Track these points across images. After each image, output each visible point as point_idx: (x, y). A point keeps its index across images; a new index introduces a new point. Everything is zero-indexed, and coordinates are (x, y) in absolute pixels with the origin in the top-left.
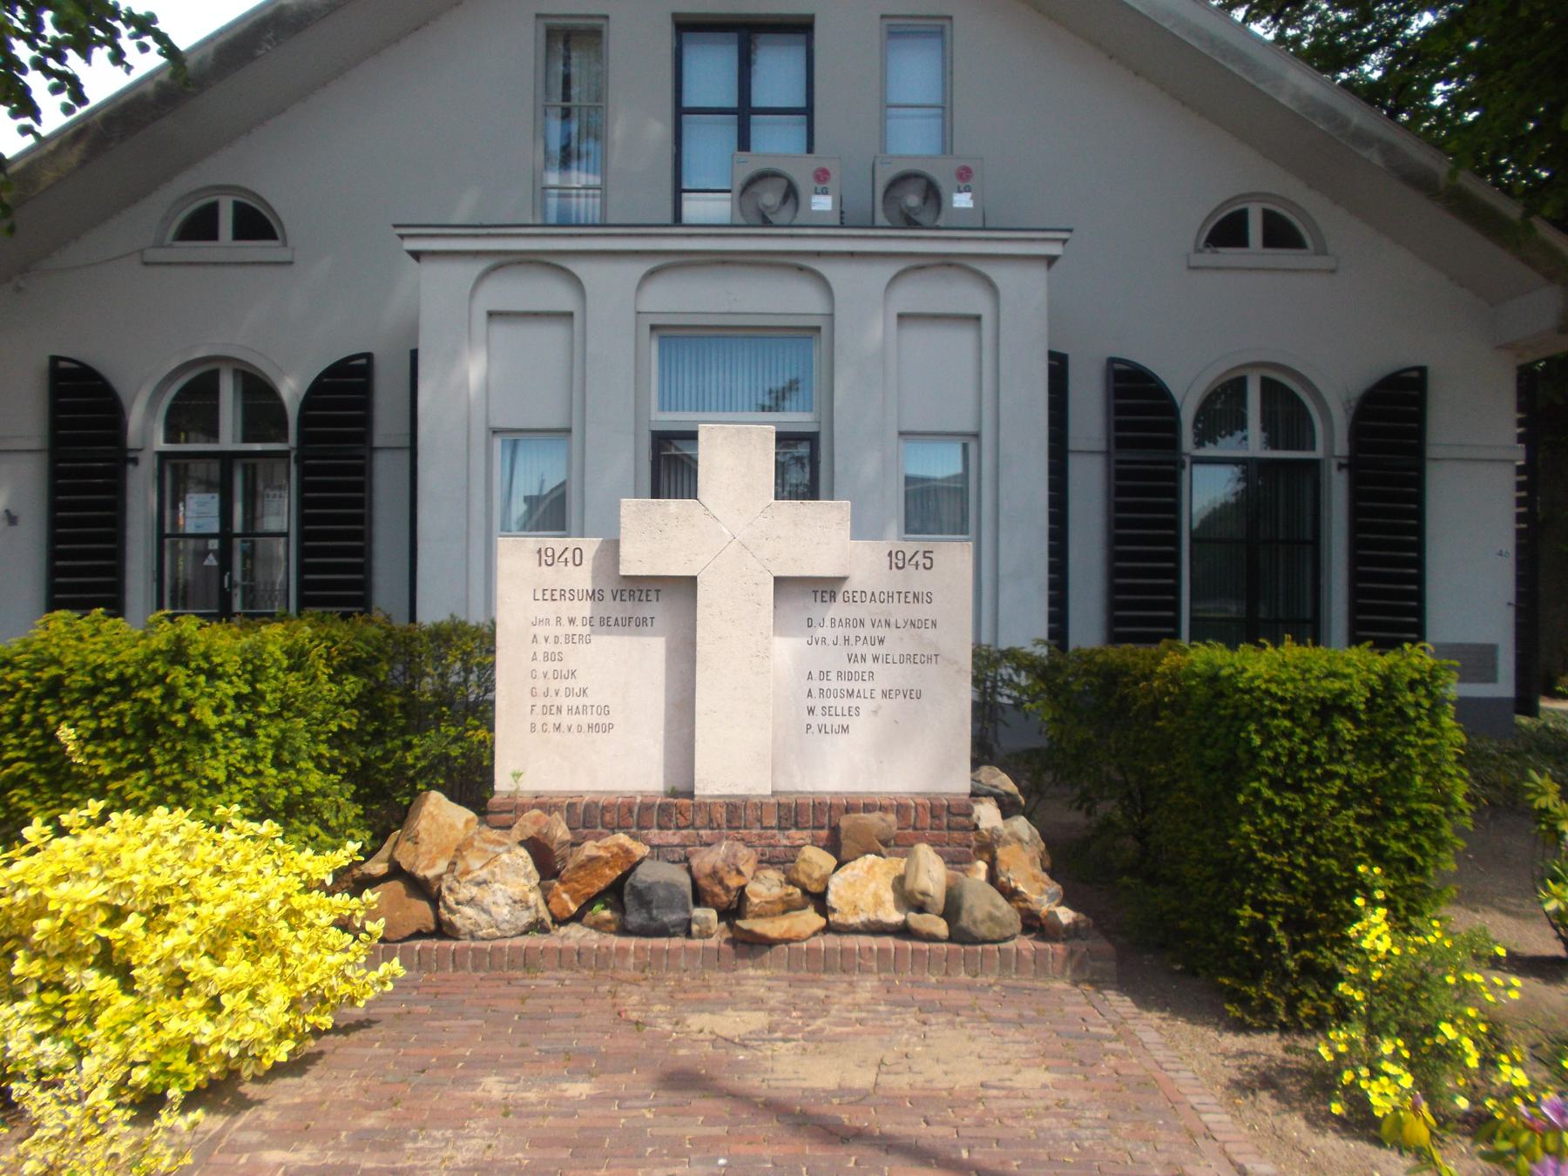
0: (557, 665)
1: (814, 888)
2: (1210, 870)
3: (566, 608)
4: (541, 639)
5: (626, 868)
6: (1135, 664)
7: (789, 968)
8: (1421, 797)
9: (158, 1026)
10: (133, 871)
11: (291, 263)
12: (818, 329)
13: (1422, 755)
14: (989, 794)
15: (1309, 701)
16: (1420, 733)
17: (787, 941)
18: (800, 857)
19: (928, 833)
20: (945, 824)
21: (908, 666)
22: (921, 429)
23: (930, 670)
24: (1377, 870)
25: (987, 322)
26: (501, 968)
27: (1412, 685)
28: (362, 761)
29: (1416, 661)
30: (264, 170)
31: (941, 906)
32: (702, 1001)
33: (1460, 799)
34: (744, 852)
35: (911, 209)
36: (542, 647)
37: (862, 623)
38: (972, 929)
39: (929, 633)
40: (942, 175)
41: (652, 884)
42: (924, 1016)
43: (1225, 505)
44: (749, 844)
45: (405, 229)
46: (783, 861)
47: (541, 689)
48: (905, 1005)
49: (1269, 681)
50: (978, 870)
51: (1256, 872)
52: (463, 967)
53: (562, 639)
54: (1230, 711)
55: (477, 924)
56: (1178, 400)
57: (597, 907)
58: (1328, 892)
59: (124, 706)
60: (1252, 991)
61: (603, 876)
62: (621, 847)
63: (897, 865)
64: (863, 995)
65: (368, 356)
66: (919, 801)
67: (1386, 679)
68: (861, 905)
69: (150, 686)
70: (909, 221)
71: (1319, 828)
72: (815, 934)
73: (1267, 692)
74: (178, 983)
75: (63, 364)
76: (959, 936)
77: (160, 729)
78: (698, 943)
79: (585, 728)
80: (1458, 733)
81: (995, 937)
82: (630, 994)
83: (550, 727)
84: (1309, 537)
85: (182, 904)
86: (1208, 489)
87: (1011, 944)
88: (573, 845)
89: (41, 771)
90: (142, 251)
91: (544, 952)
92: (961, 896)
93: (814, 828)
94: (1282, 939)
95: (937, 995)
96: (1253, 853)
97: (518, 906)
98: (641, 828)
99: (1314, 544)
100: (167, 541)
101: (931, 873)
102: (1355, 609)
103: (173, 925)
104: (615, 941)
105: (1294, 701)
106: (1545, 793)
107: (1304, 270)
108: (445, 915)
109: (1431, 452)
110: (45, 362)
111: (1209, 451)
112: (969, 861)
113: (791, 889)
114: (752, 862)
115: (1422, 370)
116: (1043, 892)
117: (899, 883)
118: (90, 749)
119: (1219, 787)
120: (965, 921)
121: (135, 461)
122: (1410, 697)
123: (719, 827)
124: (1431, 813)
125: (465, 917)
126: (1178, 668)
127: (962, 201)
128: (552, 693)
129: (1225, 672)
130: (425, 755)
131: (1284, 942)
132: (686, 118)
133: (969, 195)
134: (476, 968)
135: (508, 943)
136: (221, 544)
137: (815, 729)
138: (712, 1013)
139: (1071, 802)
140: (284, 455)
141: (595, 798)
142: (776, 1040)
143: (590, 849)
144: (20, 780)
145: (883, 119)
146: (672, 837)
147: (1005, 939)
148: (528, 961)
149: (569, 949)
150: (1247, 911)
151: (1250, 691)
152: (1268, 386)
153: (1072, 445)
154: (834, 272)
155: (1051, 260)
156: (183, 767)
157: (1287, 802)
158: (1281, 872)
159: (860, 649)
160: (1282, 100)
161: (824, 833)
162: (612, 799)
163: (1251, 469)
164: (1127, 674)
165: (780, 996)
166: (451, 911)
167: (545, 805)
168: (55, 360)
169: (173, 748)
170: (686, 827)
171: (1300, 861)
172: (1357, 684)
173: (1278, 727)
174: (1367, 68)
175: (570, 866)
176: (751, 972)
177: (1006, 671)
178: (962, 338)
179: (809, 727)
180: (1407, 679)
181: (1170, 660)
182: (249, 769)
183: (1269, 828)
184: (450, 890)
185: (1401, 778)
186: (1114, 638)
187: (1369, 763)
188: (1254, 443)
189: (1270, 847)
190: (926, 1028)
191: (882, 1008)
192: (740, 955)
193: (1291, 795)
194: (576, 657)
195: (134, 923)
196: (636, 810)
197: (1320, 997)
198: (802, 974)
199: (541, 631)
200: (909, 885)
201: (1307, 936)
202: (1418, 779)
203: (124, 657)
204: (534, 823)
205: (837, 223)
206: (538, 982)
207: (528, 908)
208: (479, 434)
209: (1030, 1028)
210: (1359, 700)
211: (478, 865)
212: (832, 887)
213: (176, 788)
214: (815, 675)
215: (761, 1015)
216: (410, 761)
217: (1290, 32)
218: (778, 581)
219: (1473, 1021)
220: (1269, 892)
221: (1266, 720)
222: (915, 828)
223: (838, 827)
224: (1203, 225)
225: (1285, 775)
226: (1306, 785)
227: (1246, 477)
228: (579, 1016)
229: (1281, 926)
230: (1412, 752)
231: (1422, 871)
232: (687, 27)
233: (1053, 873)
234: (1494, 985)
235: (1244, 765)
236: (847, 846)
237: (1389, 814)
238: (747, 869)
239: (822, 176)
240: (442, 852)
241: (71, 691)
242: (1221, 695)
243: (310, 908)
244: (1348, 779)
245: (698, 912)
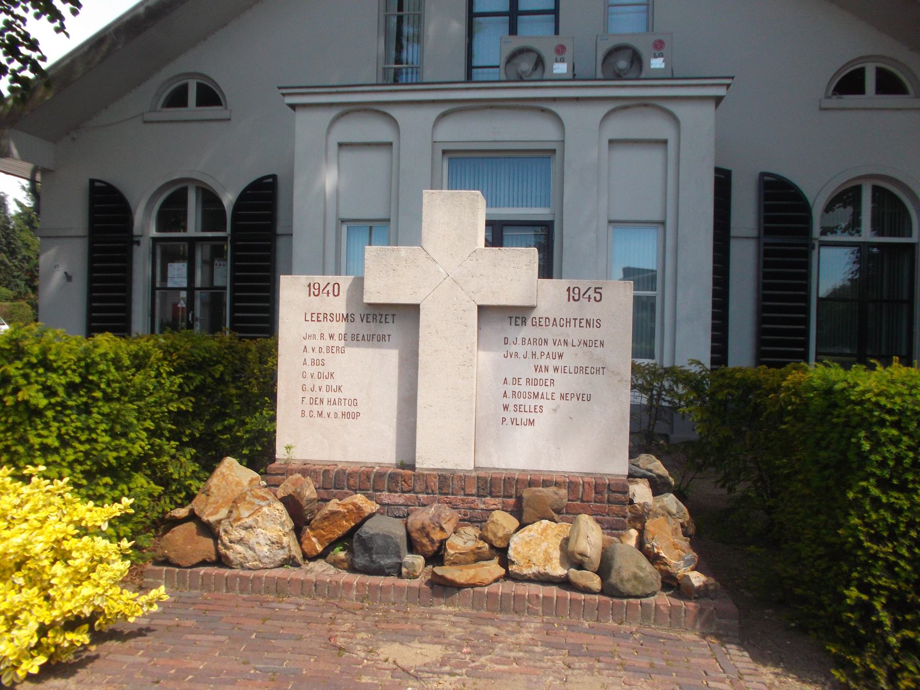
0: (321, 369)
1: (499, 544)
2: (821, 550)
3: (328, 327)
4: (309, 349)
5: (358, 521)
6: (767, 380)
11: (229, 119)
12: (554, 151)
14: (643, 476)
17: (473, 586)
18: (490, 519)
20: (603, 499)
21: (581, 376)
23: (598, 378)
25: (671, 145)
30: (214, 62)
31: (596, 565)
32: (396, 632)
34: (447, 512)
35: (621, 70)
36: (310, 356)
37: (546, 342)
38: (620, 586)
40: (643, 47)
42: (570, 659)
43: (843, 288)
44: (455, 507)
45: (286, 90)
48: (558, 647)
50: (631, 536)
51: (862, 558)
52: (233, 590)
53: (324, 350)
54: (842, 420)
55: (245, 558)
56: (811, 201)
60: (857, 660)
62: (354, 504)
63: (563, 528)
64: (525, 636)
65: (274, 177)
66: (586, 479)
68: (534, 560)
73: (877, 404)
75: (97, 184)
76: (608, 590)
78: (405, 582)
79: (340, 415)
81: (638, 593)
82: (345, 621)
83: (315, 414)
84: (905, 297)
86: (833, 270)
87: (651, 600)
90: (143, 114)
91: (290, 582)
92: (612, 558)
93: (504, 497)
94: (885, 618)
95: (585, 640)
96: (861, 542)
97: (275, 546)
98: (376, 490)
100: (157, 292)
101: (590, 537)
104: (345, 576)
105: (902, 412)
107: (905, 109)
112: (624, 528)
113: (481, 544)
116: (680, 558)
120: (614, 579)
121: (138, 243)
123: (433, 493)
125: (236, 552)
126: (800, 383)
127: (657, 63)
128: (317, 389)
129: (838, 387)
131: (888, 622)
132: (477, 19)
133: (662, 59)
135: (266, 573)
136: (188, 295)
137: (508, 421)
138: (402, 643)
139: (717, 482)
140: (225, 239)
142: (443, 673)
143: (333, 505)
145: (606, 15)
146: (399, 498)
148: (279, 588)
149: (309, 581)
150: (853, 593)
151: (861, 403)
152: (877, 191)
153: (733, 232)
154: (565, 112)
155: (718, 100)
157: (892, 500)
158: (886, 560)
159: (543, 362)
161: (512, 501)
164: (759, 388)
165: (459, 631)
166: (227, 548)
167: (306, 470)
168: (92, 181)
170: (409, 492)
171: (904, 552)
173: (886, 435)
175: (318, 517)
176: (444, 608)
178: (654, 156)
179: (504, 420)
182: (83, 438)
183: (876, 522)
184: (226, 531)
186: (759, 363)
189: (877, 538)
190: (570, 671)
191: (537, 649)
192: (436, 594)
193: (896, 494)
194: (334, 362)
196: (372, 476)
199: (310, 343)
200: (571, 547)
201: (908, 617)
204: (293, 485)
205: (571, 77)
206: (283, 605)
207: (283, 548)
209: (658, 678)
211: (247, 514)
212: (512, 545)
214: (510, 380)
215: (438, 648)
218: (481, 308)
220: (874, 577)
221: (875, 429)
222: (582, 501)
223: (522, 497)
224: (830, 83)
225: (892, 477)
226: (910, 486)
227: (859, 261)
228: (299, 638)
229: (885, 607)
235: (854, 466)
236: (528, 512)
239: (561, 50)
242: (835, 405)
243: (78, 550)
245: (409, 558)
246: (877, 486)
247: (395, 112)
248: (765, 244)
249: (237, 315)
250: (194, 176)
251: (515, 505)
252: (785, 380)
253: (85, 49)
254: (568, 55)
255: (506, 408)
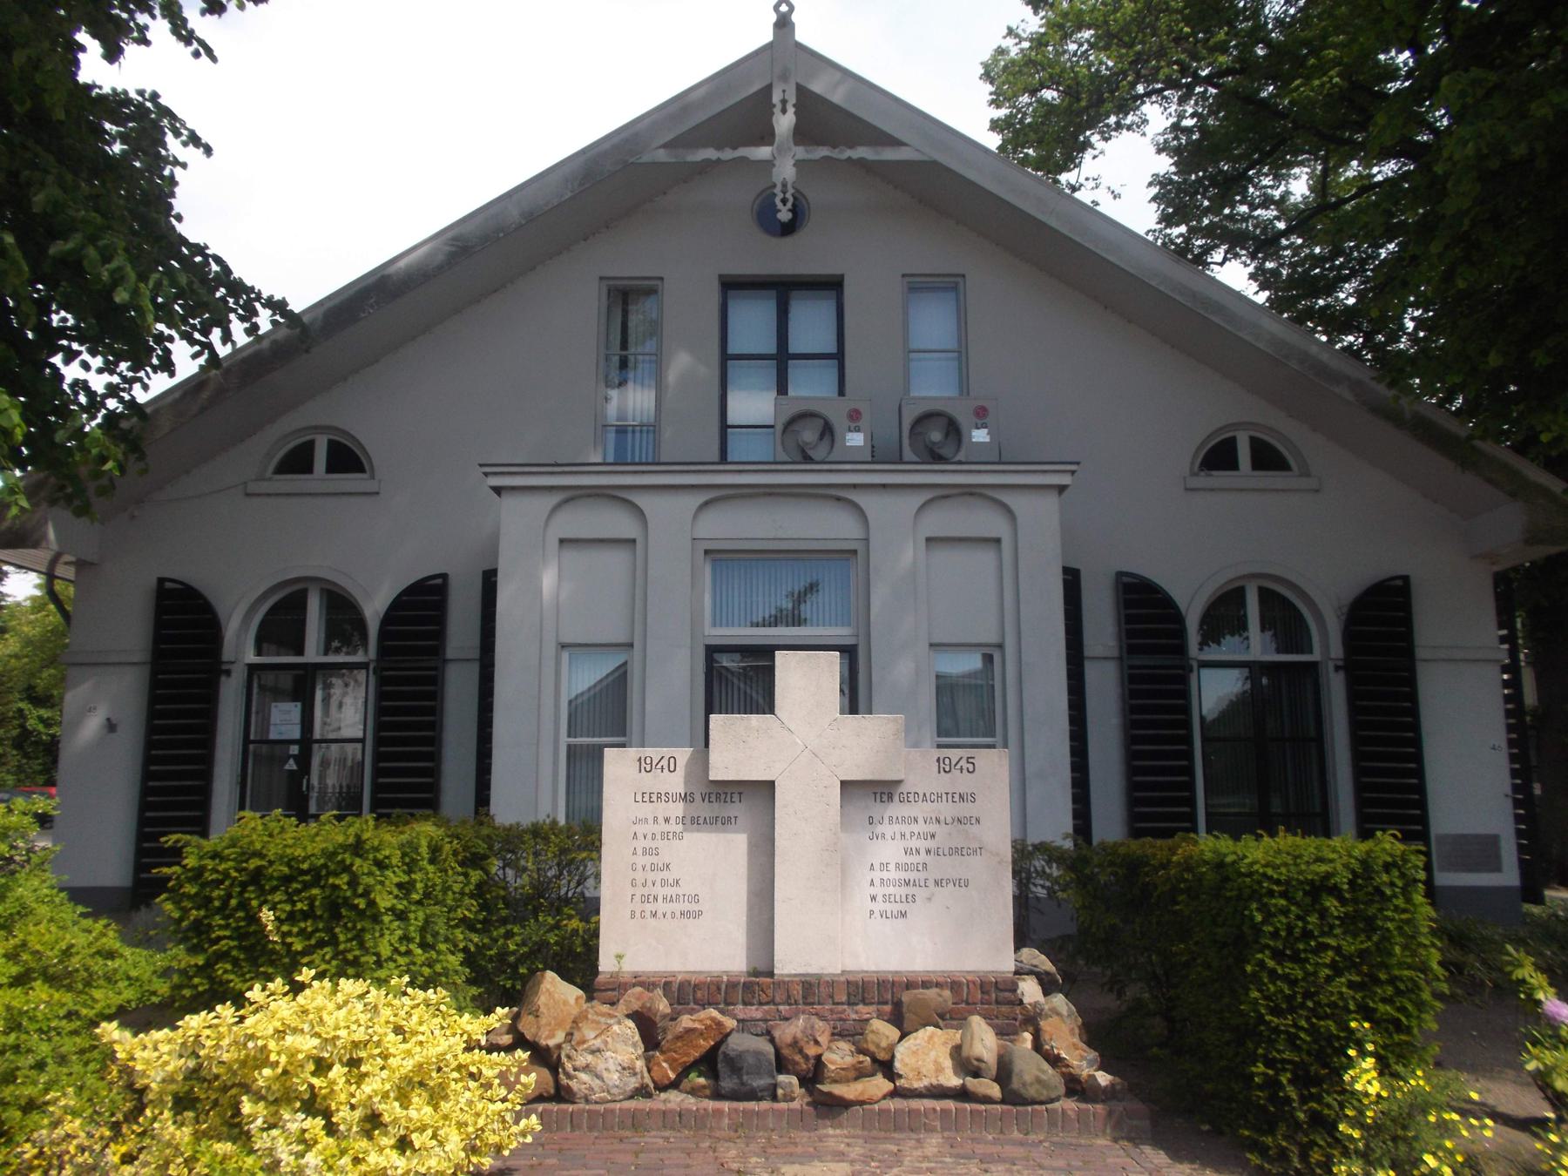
0: (654, 859)
1: (882, 1056)
2: (1227, 1036)
3: (662, 809)
4: (640, 836)
7: (863, 1128)
8: (1401, 965)
9: (357, 1161)
10: (337, 1028)
12: (855, 552)
13: (1400, 928)
14: (1030, 973)
15: (1301, 883)
16: (1396, 909)
17: (862, 1103)
18: (869, 1028)
19: (979, 1007)
20: (994, 998)
22: (954, 640)
24: (1366, 1025)
25: (1006, 545)
26: (612, 1128)
27: (1387, 867)
28: (476, 945)
29: (1388, 846)
30: (356, 413)
31: (994, 1072)
33: (1435, 966)
36: (641, 844)
37: (916, 820)
38: (1023, 1091)
39: (975, 829)
40: (963, 416)
41: (743, 1047)
42: (985, 1166)
45: (489, 468)
46: (852, 1033)
47: (639, 882)
49: (1266, 866)
50: (1025, 1040)
52: (580, 1128)
54: (1234, 893)
55: (591, 1089)
56: (1183, 607)
57: (693, 1075)
58: (1329, 1051)
59: (315, 891)
60: (1269, 1140)
61: (697, 1046)
62: (713, 1019)
63: (955, 1036)
65: (444, 576)
67: (1364, 863)
69: (336, 875)
70: (935, 456)
71: (1317, 993)
72: (884, 1097)
73: (1264, 875)
74: (373, 1122)
75: (168, 585)
77: (344, 912)
78: (783, 1105)
80: (1429, 908)
82: (728, 1149)
83: (648, 914)
84: (1313, 733)
85: (373, 1057)
86: (1215, 690)
87: (1057, 1105)
88: (673, 1019)
89: (240, 948)
92: (1011, 1062)
93: (879, 1003)
96: (1261, 1016)
98: (727, 1004)
99: (1318, 741)
100: (251, 747)
101: (984, 1041)
102: (1361, 803)
103: (366, 1075)
104: (711, 1105)
105: (1288, 882)
106: (1521, 966)
108: (564, 1080)
109: (1420, 653)
110: (154, 581)
111: (1212, 654)
112: (1016, 1033)
113: (861, 1057)
114: (827, 1034)
115: (1406, 579)
116: (1082, 1058)
117: (956, 1051)
118: (285, 928)
119: (1231, 960)
120: (1015, 1084)
122: (1385, 877)
123: (796, 1003)
124: (1411, 979)
125: (581, 1082)
127: (980, 436)
128: (649, 883)
129: (1229, 859)
130: (524, 944)
131: (1294, 1096)
132: (730, 363)
134: (591, 1129)
135: (618, 1105)
137: (877, 914)
138: (801, 1164)
141: (687, 977)
143: (686, 1021)
144: (223, 956)
146: (754, 1012)
147: (1052, 1101)
148: (636, 1122)
149: (671, 1111)
150: (1261, 1068)
151: (1250, 874)
152: (1266, 596)
153: (1088, 652)
155: (1061, 489)
156: (362, 945)
158: (1287, 1032)
160: (1261, 345)
161: (888, 1008)
162: (702, 978)
163: (1255, 669)
164: (1147, 864)
166: (569, 1077)
168: (161, 581)
169: (354, 927)
170: (767, 1003)
171: (1303, 1023)
172: (1339, 867)
174: (1342, 296)
175: (669, 1037)
176: (831, 1131)
177: (1039, 863)
178: (984, 559)
180: (1380, 862)
181: (1184, 850)
182: (403, 949)
183: (1274, 994)
184: (569, 1057)
185: (1383, 948)
186: (1135, 833)
187: (1355, 936)
188: (1258, 645)
192: (819, 1116)
194: (671, 851)
195: (338, 1072)
197: (1329, 1145)
198: (875, 1133)
199: (641, 829)
200: (965, 1052)
201: (1313, 1090)
202: (1397, 949)
203: (309, 850)
207: (635, 1074)
208: (550, 649)
210: (1342, 880)
212: (898, 1056)
213: (355, 962)
214: (877, 866)
216: (512, 947)
217: (1269, 265)
218: (843, 783)
219: (1451, 1153)
220: (1279, 1051)
222: (968, 1003)
223: (899, 1000)
224: (1192, 463)
228: (688, 1166)
229: (1290, 1081)
230: (1389, 925)
231: (1408, 1030)
232: (732, 286)
233: (1090, 1044)
234: (1472, 1126)
237: (1377, 981)
238: (823, 1039)
239: (855, 415)
240: (560, 1025)
241: (271, 878)
242: (1226, 879)
244: (1338, 950)
246: (1273, 958)
247: (641, 500)
248: (1131, 667)
249: (381, 780)
250: (321, 574)
251: (892, 1013)
252: (1174, 854)
253: (177, 395)
254: (864, 422)
255: (873, 898)
